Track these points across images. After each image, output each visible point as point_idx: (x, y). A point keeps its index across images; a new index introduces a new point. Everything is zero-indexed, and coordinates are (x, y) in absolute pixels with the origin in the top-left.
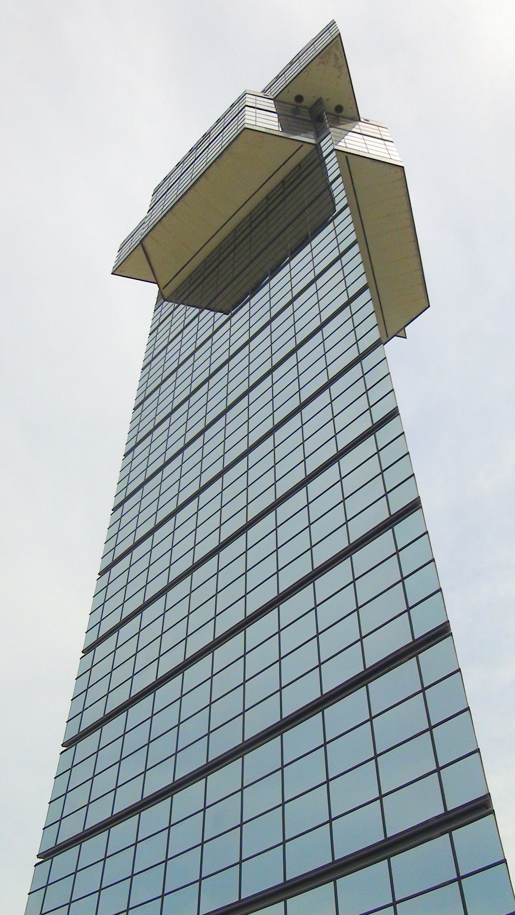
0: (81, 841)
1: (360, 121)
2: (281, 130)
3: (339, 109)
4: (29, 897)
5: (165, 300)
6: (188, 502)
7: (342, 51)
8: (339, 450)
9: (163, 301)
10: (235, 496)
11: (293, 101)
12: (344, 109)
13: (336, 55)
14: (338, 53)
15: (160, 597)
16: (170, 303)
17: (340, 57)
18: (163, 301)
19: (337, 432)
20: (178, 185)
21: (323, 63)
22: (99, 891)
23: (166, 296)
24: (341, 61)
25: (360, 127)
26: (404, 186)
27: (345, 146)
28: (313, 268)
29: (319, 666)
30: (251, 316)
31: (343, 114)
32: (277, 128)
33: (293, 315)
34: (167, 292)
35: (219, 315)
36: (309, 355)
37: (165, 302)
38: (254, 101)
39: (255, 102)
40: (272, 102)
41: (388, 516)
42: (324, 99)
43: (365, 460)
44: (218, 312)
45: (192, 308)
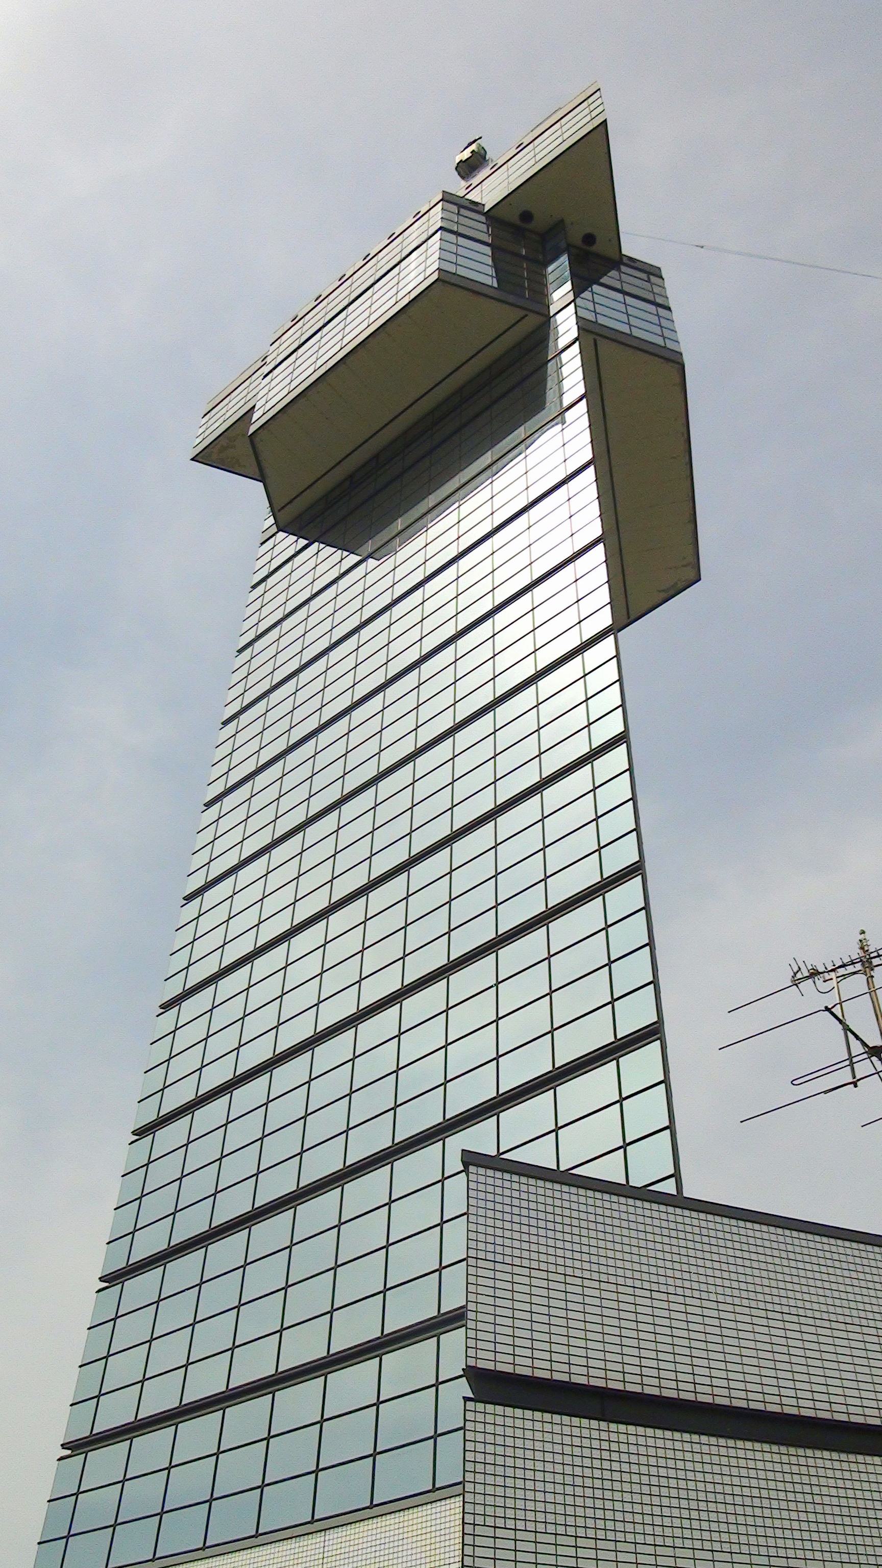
0: (165, 1261)
2: (496, 285)
4: (89, 1333)
5: (279, 530)
8: (451, 959)
9: (276, 530)
10: (117, 1392)
16: (291, 536)
18: (276, 530)
19: (494, 849)
20: (246, 391)
22: (256, 1175)
23: (281, 525)
26: (683, 424)
28: (412, 782)
29: (444, 1084)
30: (304, 849)
32: (488, 281)
33: (323, 948)
34: (284, 516)
36: (200, 1274)
37: (281, 533)
41: (441, 1120)
43: (433, 1050)
45: (490, 259)
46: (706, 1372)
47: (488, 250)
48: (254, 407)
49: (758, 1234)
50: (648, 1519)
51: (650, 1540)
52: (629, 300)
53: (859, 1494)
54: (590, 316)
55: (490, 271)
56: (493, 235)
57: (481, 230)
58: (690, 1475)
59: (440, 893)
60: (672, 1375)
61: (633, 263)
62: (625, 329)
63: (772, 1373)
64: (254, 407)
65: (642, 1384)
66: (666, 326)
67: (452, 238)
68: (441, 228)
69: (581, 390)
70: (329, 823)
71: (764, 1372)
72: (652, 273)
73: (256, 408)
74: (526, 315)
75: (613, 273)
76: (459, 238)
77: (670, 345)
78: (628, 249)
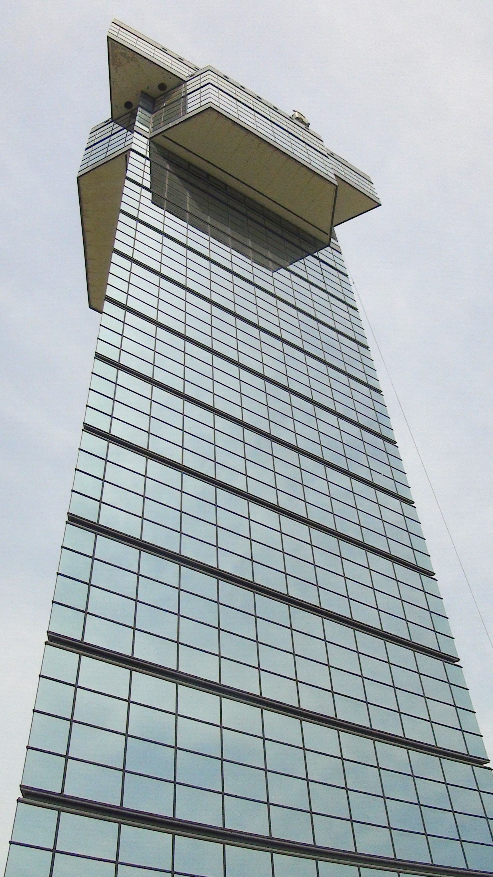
1: (186, 82)
3: (162, 87)
6: (196, 252)
7: (122, 46)
11: (126, 110)
12: (166, 84)
13: (121, 54)
14: (122, 51)
15: (376, 554)
17: (126, 52)
21: (119, 66)
24: (129, 54)
25: (191, 86)
27: (237, 112)
31: (168, 89)
35: (117, 125)
38: (120, 32)
39: (120, 31)
40: (146, 141)
42: (144, 89)
44: (151, 183)
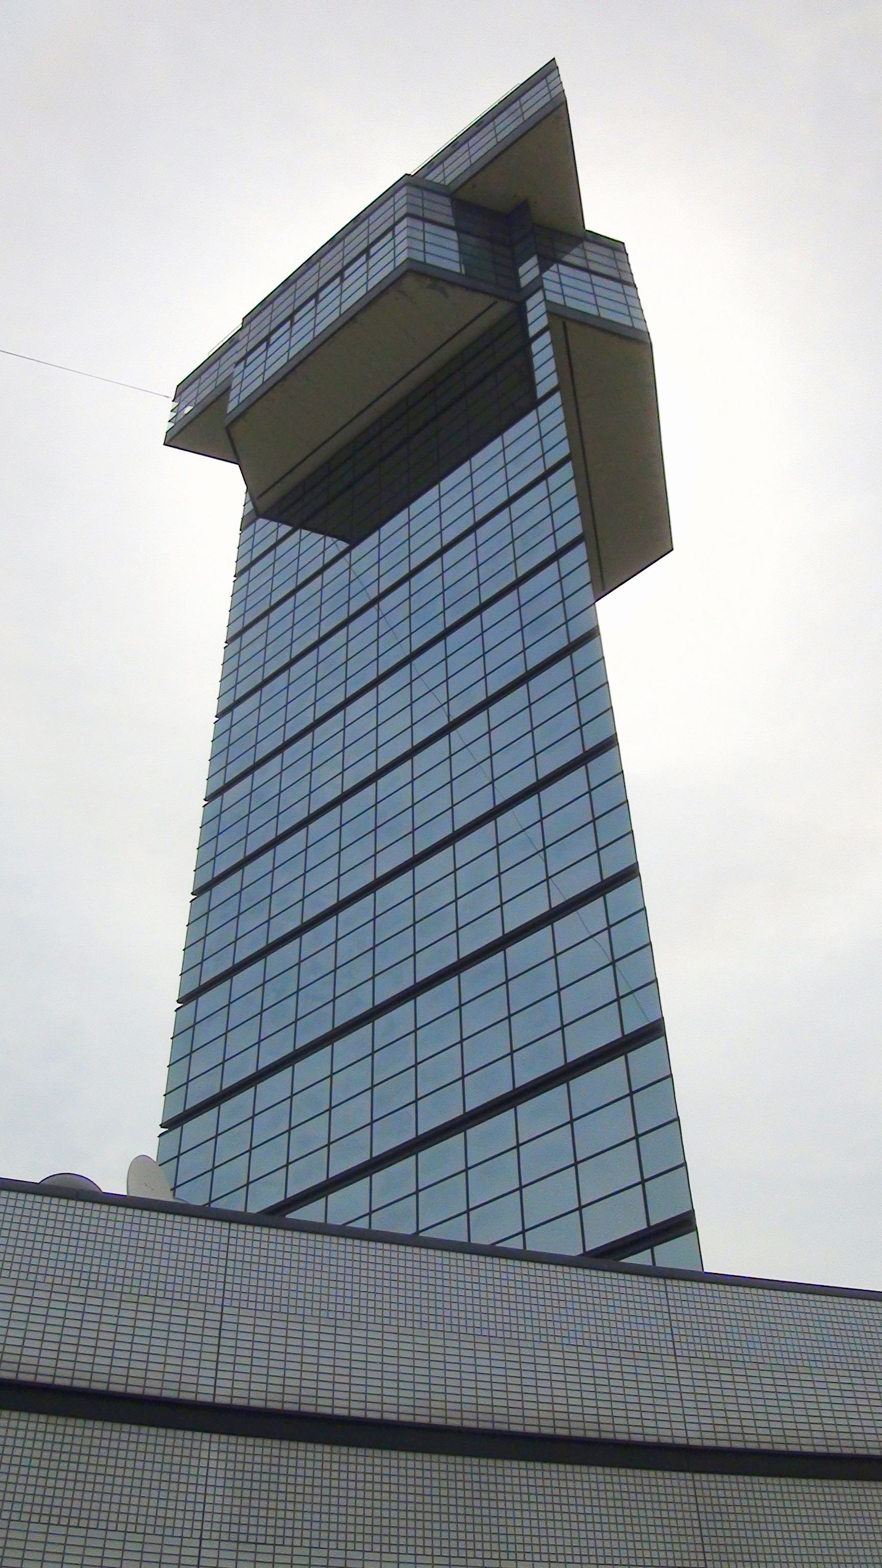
32: (456, 268)
46: (763, 1409)
47: (453, 235)
48: (232, 374)
49: (825, 1305)
50: (571, 1320)
51: (573, 1342)
52: (596, 279)
53: (769, 1306)
54: (558, 299)
55: (456, 256)
56: (456, 217)
57: (443, 210)
58: (641, 1327)
59: (404, 799)
60: (738, 1422)
61: (598, 239)
62: (593, 311)
63: (812, 1392)
64: (232, 374)
65: (716, 1439)
66: (632, 304)
67: (419, 224)
68: (407, 215)
69: (535, 347)
70: (304, 744)
71: (806, 1391)
72: (616, 248)
73: (234, 375)
74: (495, 303)
75: (576, 251)
76: (421, 215)
77: (638, 324)
78: (591, 224)
